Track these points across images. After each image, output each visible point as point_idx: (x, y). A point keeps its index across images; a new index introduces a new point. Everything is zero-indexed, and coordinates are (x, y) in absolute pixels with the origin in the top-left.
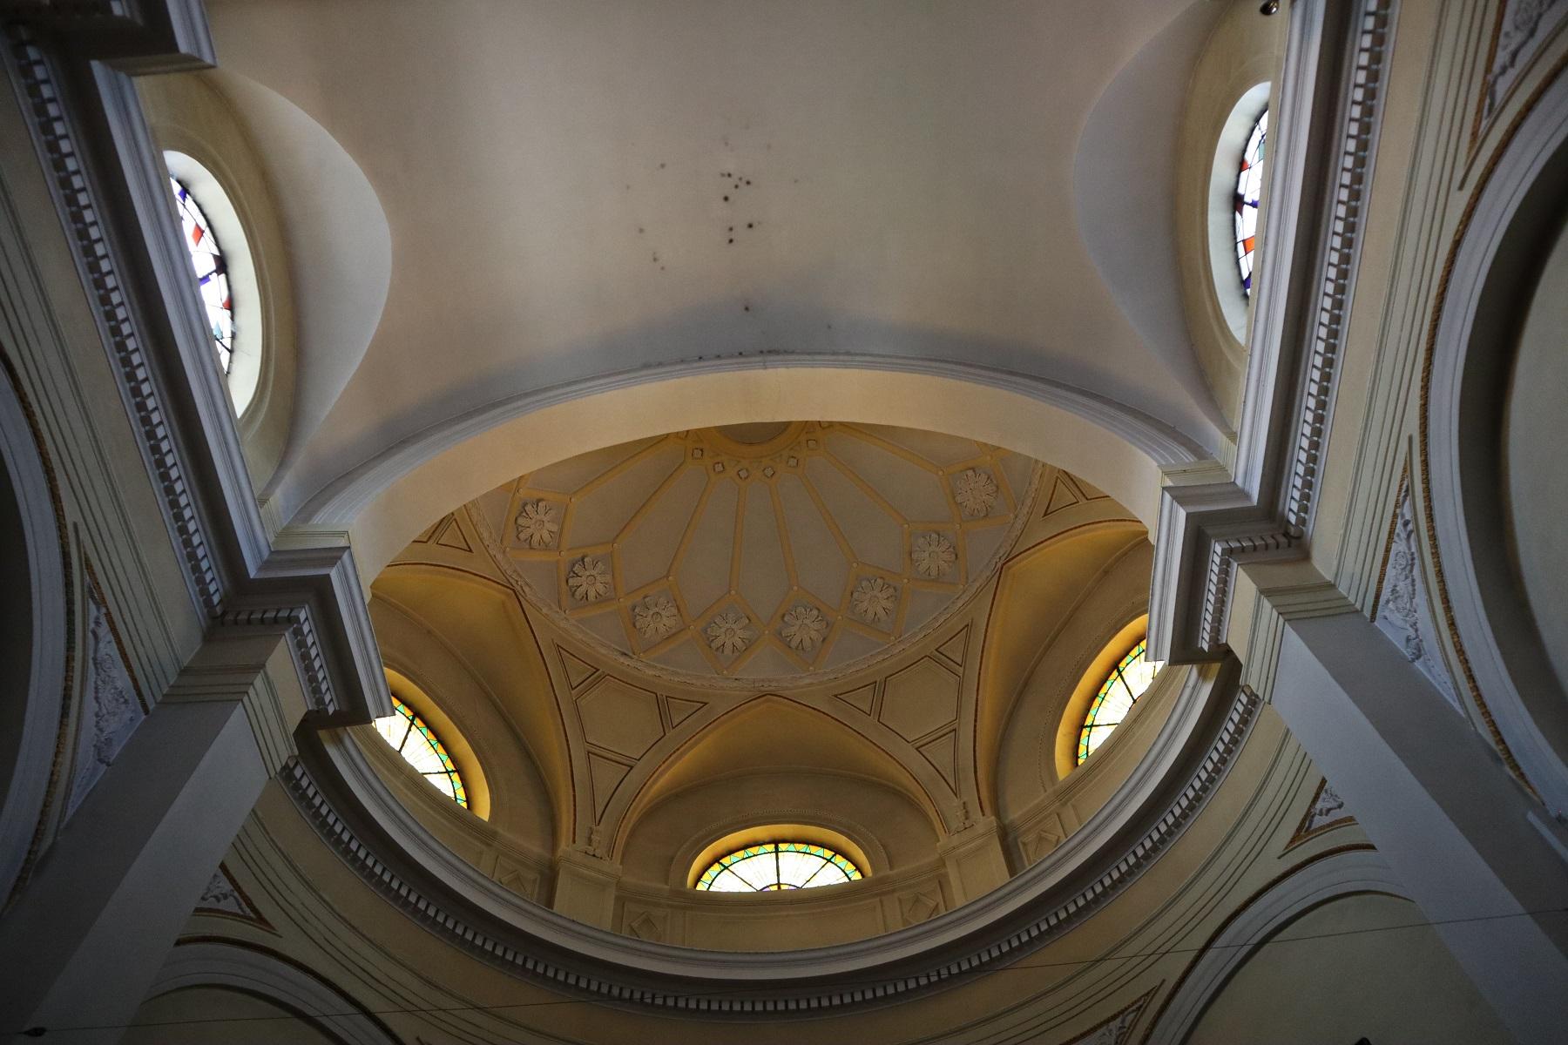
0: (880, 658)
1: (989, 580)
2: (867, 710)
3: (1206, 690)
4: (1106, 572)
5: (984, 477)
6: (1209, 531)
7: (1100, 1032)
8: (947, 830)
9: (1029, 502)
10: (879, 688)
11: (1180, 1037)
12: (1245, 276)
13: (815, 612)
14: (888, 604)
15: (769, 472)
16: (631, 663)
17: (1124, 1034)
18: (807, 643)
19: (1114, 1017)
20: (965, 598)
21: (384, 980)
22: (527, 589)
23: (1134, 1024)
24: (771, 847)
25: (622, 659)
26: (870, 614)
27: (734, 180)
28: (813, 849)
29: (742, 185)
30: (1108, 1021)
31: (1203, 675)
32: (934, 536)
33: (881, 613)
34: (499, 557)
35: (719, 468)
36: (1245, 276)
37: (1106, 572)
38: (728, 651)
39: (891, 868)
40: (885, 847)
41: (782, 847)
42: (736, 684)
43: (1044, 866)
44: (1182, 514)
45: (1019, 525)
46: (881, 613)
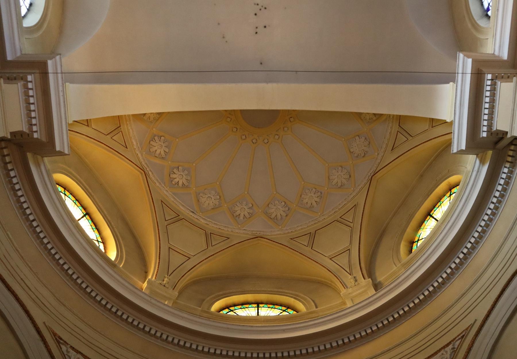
0: (313, 223)
1: (365, 184)
2: (306, 244)
3: (485, 169)
4: (422, 176)
5: (364, 138)
6: (484, 70)
7: (440, 354)
8: (345, 286)
9: (384, 146)
10: (312, 236)
11: (486, 355)
12: (486, 6)
13: (283, 203)
14: (317, 199)
15: (266, 141)
16: (195, 216)
17: (455, 351)
18: (279, 217)
19: (448, 345)
20: (354, 194)
21: (33, 290)
22: (150, 173)
23: (460, 345)
24: (256, 305)
25: (191, 214)
26: (309, 205)
27: (260, 7)
28: (276, 307)
29: (263, 9)
30: (444, 347)
31: (482, 162)
32: (340, 168)
33: (314, 204)
34: (139, 155)
35: (244, 137)
36: (486, 6)
37: (422, 176)
38: (242, 217)
39: (317, 307)
40: (313, 301)
41: (260, 305)
42: (244, 231)
43: (400, 279)
44: (470, 61)
45: (380, 157)
46: (314, 204)
